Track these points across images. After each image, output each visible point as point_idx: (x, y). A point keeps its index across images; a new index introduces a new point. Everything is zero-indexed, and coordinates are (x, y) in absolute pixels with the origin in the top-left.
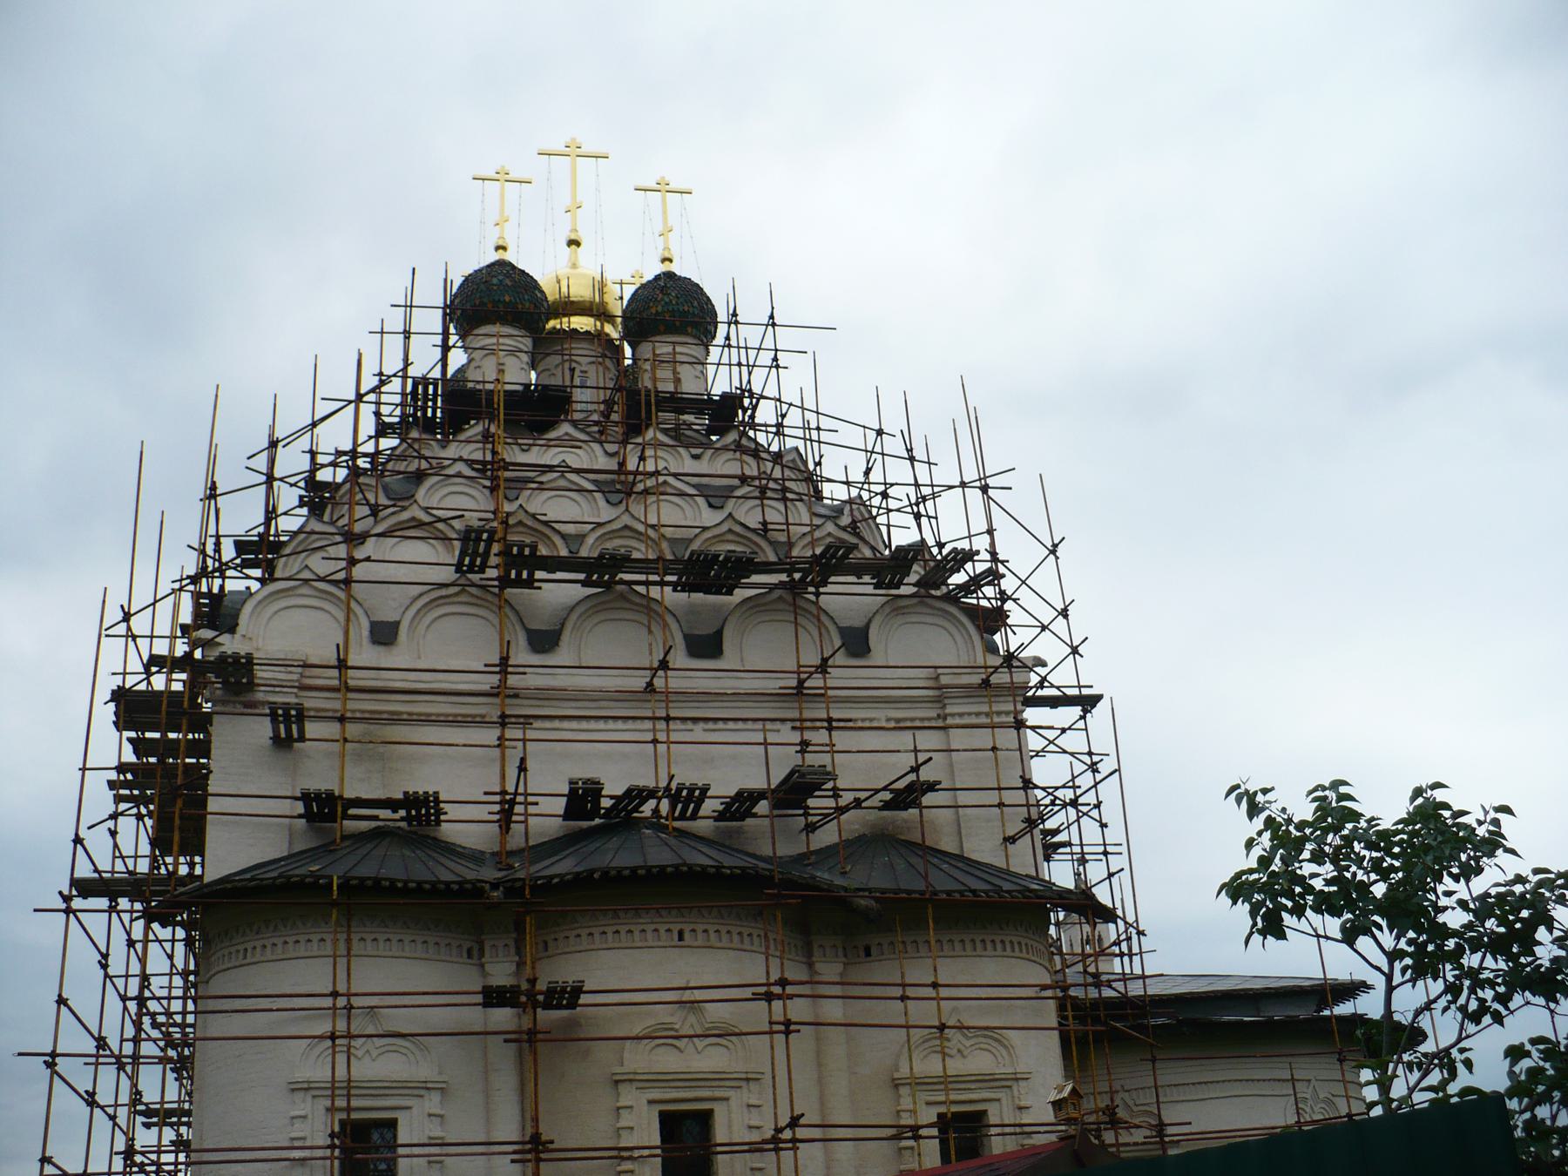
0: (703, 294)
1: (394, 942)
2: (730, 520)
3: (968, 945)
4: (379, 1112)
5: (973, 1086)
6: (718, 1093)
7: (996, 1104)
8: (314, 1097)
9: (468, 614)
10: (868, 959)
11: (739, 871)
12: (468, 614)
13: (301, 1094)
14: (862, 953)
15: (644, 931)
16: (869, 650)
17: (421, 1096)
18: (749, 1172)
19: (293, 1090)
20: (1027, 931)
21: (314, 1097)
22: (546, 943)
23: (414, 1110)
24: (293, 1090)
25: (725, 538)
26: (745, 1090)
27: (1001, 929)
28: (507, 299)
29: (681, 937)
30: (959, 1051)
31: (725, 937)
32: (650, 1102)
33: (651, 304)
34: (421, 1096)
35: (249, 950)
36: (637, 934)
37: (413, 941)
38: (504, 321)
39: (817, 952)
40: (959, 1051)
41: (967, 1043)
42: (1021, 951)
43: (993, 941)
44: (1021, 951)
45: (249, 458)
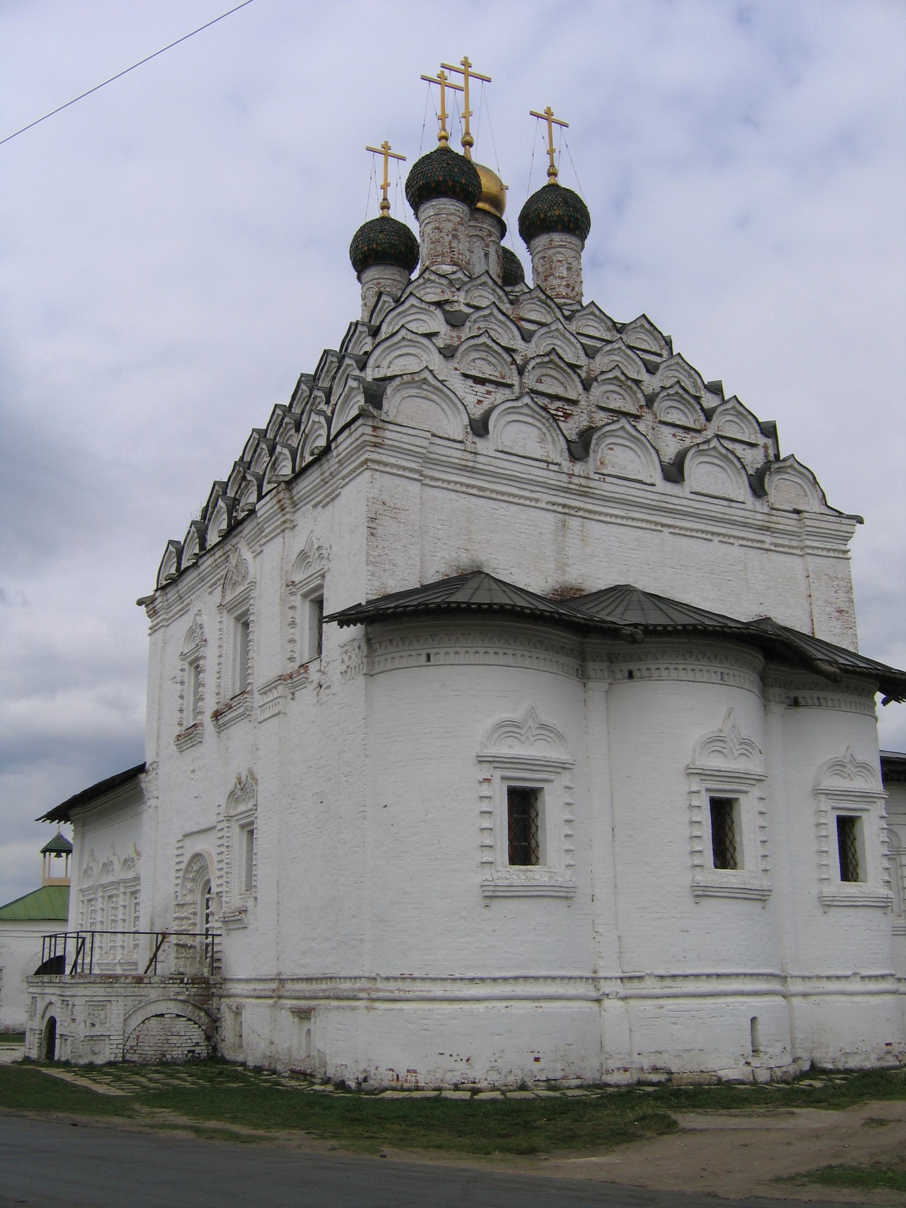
0: (587, 210)
1: (501, 654)
4: (732, 793)
6: (744, 788)
9: (526, 423)
11: (557, 616)
12: (526, 423)
13: (487, 765)
15: (648, 669)
16: (684, 480)
17: (559, 773)
18: (563, 838)
19: (480, 761)
22: (428, 656)
23: (750, 795)
24: (480, 761)
27: (860, 695)
28: (464, 181)
33: (555, 208)
34: (559, 773)
37: (486, 652)
38: (445, 194)
40: (849, 775)
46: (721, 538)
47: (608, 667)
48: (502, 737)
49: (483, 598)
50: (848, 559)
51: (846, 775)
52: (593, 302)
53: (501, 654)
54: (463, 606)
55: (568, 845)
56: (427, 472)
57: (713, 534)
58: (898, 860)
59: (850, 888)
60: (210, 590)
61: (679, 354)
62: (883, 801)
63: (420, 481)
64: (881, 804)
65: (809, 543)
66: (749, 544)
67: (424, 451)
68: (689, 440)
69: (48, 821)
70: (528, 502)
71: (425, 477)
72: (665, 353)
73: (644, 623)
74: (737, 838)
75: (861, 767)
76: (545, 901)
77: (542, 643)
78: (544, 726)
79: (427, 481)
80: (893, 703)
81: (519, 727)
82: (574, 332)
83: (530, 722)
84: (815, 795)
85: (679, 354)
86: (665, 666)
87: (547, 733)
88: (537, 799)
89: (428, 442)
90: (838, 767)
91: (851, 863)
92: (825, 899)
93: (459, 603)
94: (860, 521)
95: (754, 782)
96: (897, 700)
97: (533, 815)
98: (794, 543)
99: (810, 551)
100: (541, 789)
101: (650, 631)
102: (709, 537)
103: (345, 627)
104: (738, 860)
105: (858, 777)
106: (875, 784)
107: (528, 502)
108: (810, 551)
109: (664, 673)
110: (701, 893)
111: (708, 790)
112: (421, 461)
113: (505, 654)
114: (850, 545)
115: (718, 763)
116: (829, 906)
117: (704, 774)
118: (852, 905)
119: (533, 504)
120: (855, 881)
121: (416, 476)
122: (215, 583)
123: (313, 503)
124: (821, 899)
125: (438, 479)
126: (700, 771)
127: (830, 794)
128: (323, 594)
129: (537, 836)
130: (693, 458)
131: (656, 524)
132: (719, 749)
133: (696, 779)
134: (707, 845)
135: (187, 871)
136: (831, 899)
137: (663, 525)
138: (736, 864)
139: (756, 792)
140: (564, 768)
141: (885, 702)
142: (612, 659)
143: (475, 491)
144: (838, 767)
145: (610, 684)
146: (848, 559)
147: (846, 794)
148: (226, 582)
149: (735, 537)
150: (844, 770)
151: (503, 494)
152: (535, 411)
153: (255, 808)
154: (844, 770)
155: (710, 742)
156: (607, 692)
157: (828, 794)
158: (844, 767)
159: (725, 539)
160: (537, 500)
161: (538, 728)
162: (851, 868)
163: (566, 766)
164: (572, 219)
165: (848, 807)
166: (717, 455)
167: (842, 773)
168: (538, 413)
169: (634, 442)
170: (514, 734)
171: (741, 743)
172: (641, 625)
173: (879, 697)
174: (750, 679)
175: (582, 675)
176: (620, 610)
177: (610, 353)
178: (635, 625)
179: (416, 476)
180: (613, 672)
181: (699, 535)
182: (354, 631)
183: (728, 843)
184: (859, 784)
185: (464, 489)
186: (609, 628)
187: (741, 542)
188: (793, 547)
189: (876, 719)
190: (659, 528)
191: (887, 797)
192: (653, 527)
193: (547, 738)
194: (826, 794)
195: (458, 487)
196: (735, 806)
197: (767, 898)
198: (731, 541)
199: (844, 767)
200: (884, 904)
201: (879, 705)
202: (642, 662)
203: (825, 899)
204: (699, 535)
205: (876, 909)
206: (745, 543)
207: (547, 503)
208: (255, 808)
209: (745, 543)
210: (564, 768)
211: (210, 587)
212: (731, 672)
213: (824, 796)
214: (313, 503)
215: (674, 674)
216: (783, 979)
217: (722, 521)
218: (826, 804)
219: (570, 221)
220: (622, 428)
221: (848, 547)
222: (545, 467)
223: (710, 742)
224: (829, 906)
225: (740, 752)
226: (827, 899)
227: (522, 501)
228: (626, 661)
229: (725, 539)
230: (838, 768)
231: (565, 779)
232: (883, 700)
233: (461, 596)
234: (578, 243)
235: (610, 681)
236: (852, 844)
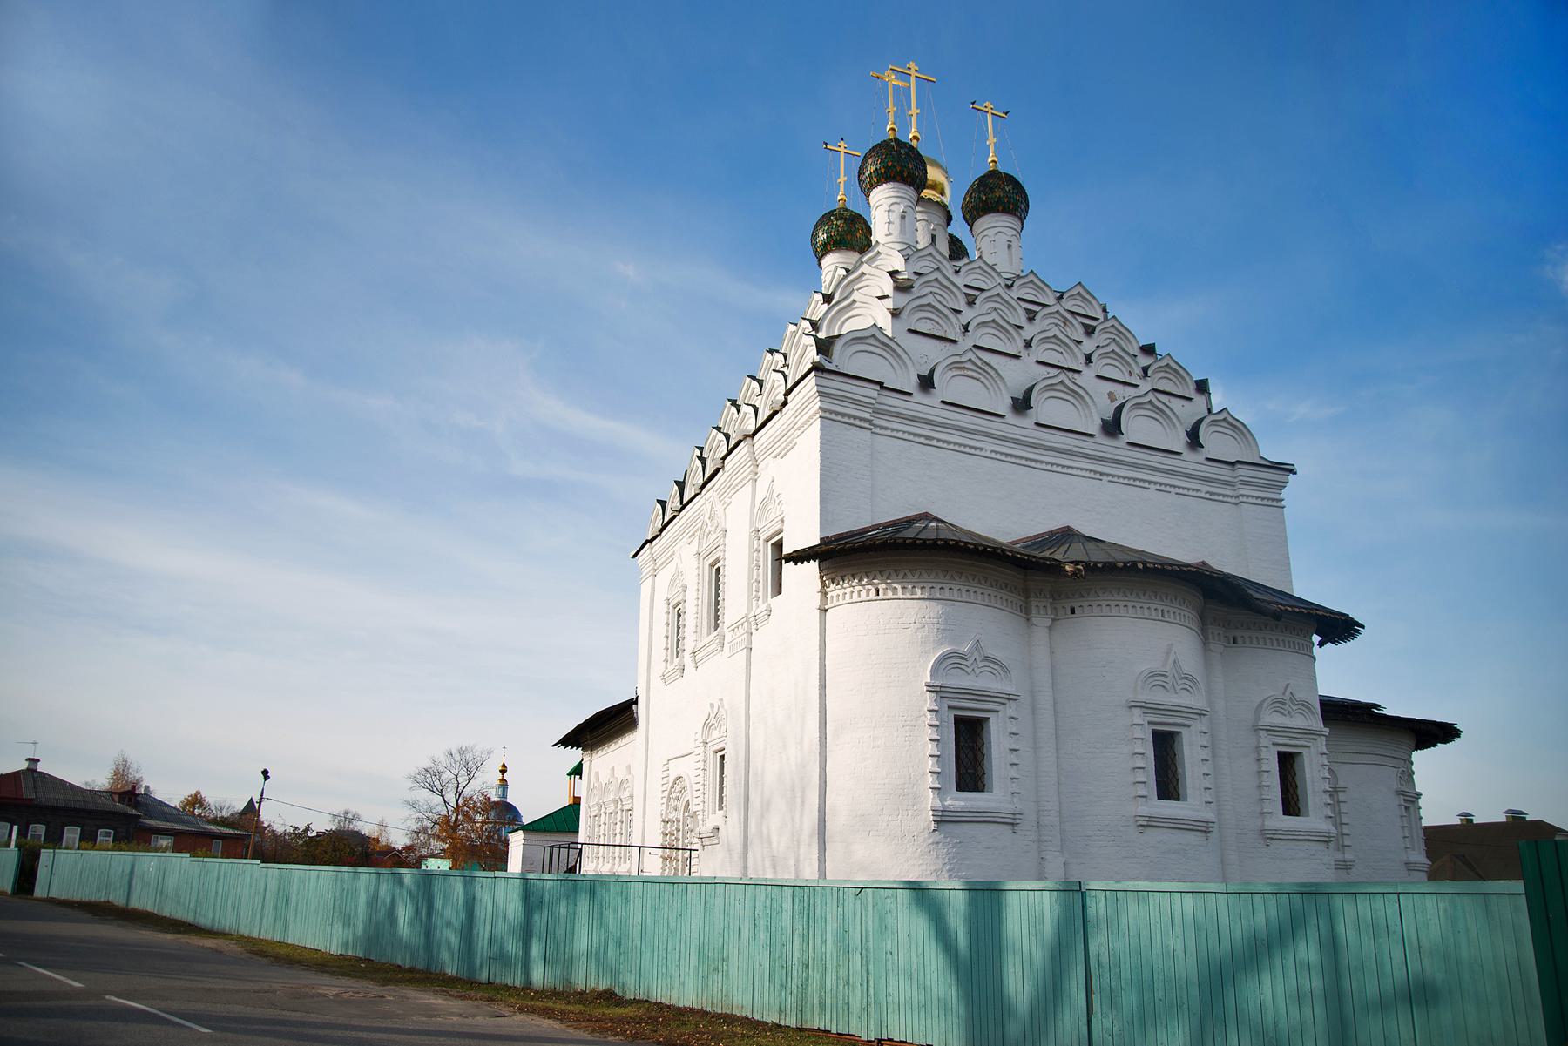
2: (1031, 275)
3: (1261, 641)
5: (1299, 736)
6: (1186, 722)
7: (1306, 749)
8: (941, 697)
10: (1073, 615)
14: (1069, 611)
19: (1131, 707)
20: (1187, 607)
21: (941, 697)
24: (1131, 707)
25: (1108, 330)
26: (1198, 721)
29: (1235, 641)
30: (1289, 712)
31: (980, 597)
32: (950, 707)
35: (835, 597)
36: (955, 591)
39: (1034, 611)
40: (1289, 712)
41: (1295, 708)
42: (1185, 621)
43: (1277, 640)
44: (1303, 650)
45: (1017, 357)
46: (1158, 487)
47: (1051, 604)
48: (948, 668)
49: (929, 535)
50: (1283, 507)
51: (1286, 713)
52: (1032, 272)
53: (947, 590)
54: (907, 541)
55: (1015, 787)
56: (876, 421)
57: (1150, 482)
58: (1336, 797)
59: (1291, 822)
60: (690, 540)
61: (1114, 317)
62: (1324, 738)
63: (871, 429)
64: (1321, 745)
65: (1242, 492)
66: (1186, 492)
67: (873, 401)
68: (1122, 393)
69: (562, 747)
70: (972, 451)
71: (876, 426)
72: (1100, 316)
73: (1086, 559)
74: (1180, 770)
75: (1302, 705)
76: (991, 827)
77: (986, 579)
78: (988, 659)
79: (877, 430)
80: (1329, 645)
81: (965, 659)
82: (1015, 298)
83: (976, 654)
84: (1255, 730)
85: (1114, 317)
86: (1107, 603)
87: (992, 665)
88: (983, 728)
89: (878, 400)
90: (1279, 704)
91: (1293, 798)
92: (1267, 832)
93: (905, 539)
94: (1293, 472)
95: (1196, 717)
96: (1334, 643)
97: (979, 744)
98: (1228, 492)
99: (1245, 499)
100: (988, 719)
101: (1091, 568)
102: (1146, 485)
103: (799, 564)
104: (1181, 792)
105: (1298, 714)
106: (1317, 723)
107: (972, 451)
108: (1245, 499)
109: (1105, 610)
110: (1148, 823)
111: (1149, 723)
112: (871, 411)
113: (950, 589)
114: (1284, 494)
115: (1160, 697)
116: (1272, 839)
117: (1146, 708)
118: (1294, 838)
119: (978, 452)
120: (1298, 816)
121: (867, 425)
122: (694, 534)
123: (773, 455)
124: (1263, 832)
125: (886, 428)
126: (1143, 704)
127: (1270, 730)
128: (782, 538)
129: (983, 764)
130: (1130, 411)
131: (1095, 472)
132: (1161, 683)
133: (1137, 712)
134: (1150, 776)
135: (671, 793)
136: (1274, 832)
137: (1102, 474)
138: (1179, 795)
139: (1199, 725)
140: (1009, 699)
141: (1321, 644)
142: (1055, 596)
143: (922, 440)
144: (1279, 704)
145: (1053, 620)
146: (1283, 507)
147: (1286, 730)
148: (703, 533)
149: (1171, 486)
150: (1283, 707)
151: (949, 443)
152: (976, 365)
153: (725, 734)
154: (1283, 707)
155: (1153, 676)
156: (1050, 628)
157: (1270, 730)
158: (1285, 704)
159: (1163, 488)
160: (982, 449)
161: (983, 660)
162: (1293, 803)
163: (1011, 697)
164: (1012, 200)
165: (1289, 743)
166: (1152, 408)
167: (1283, 711)
168: (980, 368)
169: (1073, 396)
170: (959, 666)
171: (1183, 678)
172: (1082, 562)
173: (1316, 639)
174: (1190, 615)
175: (1026, 612)
176: (1063, 549)
177: (1048, 388)
178: (1076, 563)
179: (867, 425)
180: (1055, 608)
181: (1137, 483)
182: (812, 567)
183: (1170, 776)
184: (1298, 721)
185: (911, 437)
186: (1051, 565)
187: (1177, 490)
188: (1227, 496)
189: (1315, 659)
190: (1098, 476)
191: (1327, 734)
192: (1092, 475)
193: (992, 671)
194: (1267, 730)
195: (906, 436)
196: (1177, 739)
197: (1211, 829)
198: (1168, 489)
199: (1285, 704)
200: (1327, 839)
201: (1316, 649)
202: (1085, 599)
203: (1267, 832)
204: (1137, 483)
205: (1318, 843)
206: (1181, 491)
207: (991, 451)
208: (725, 734)
209: (1181, 491)
210: (1009, 699)
211: (690, 537)
212: (1172, 610)
213: (1264, 732)
214: (773, 455)
215: (1114, 611)
216: (1345, 862)
217: (1159, 470)
218: (1266, 740)
219: (1009, 202)
220: (1062, 382)
221: (1282, 496)
222: (967, 261)
223: (1153, 676)
224: (1272, 839)
225: (1181, 687)
226: (1270, 832)
227: (967, 450)
228: (1069, 598)
229: (1163, 488)
230: (1278, 705)
231: (1010, 709)
232: (1320, 641)
233: (909, 534)
234: (1018, 225)
235: (1053, 616)
236: (1293, 778)
